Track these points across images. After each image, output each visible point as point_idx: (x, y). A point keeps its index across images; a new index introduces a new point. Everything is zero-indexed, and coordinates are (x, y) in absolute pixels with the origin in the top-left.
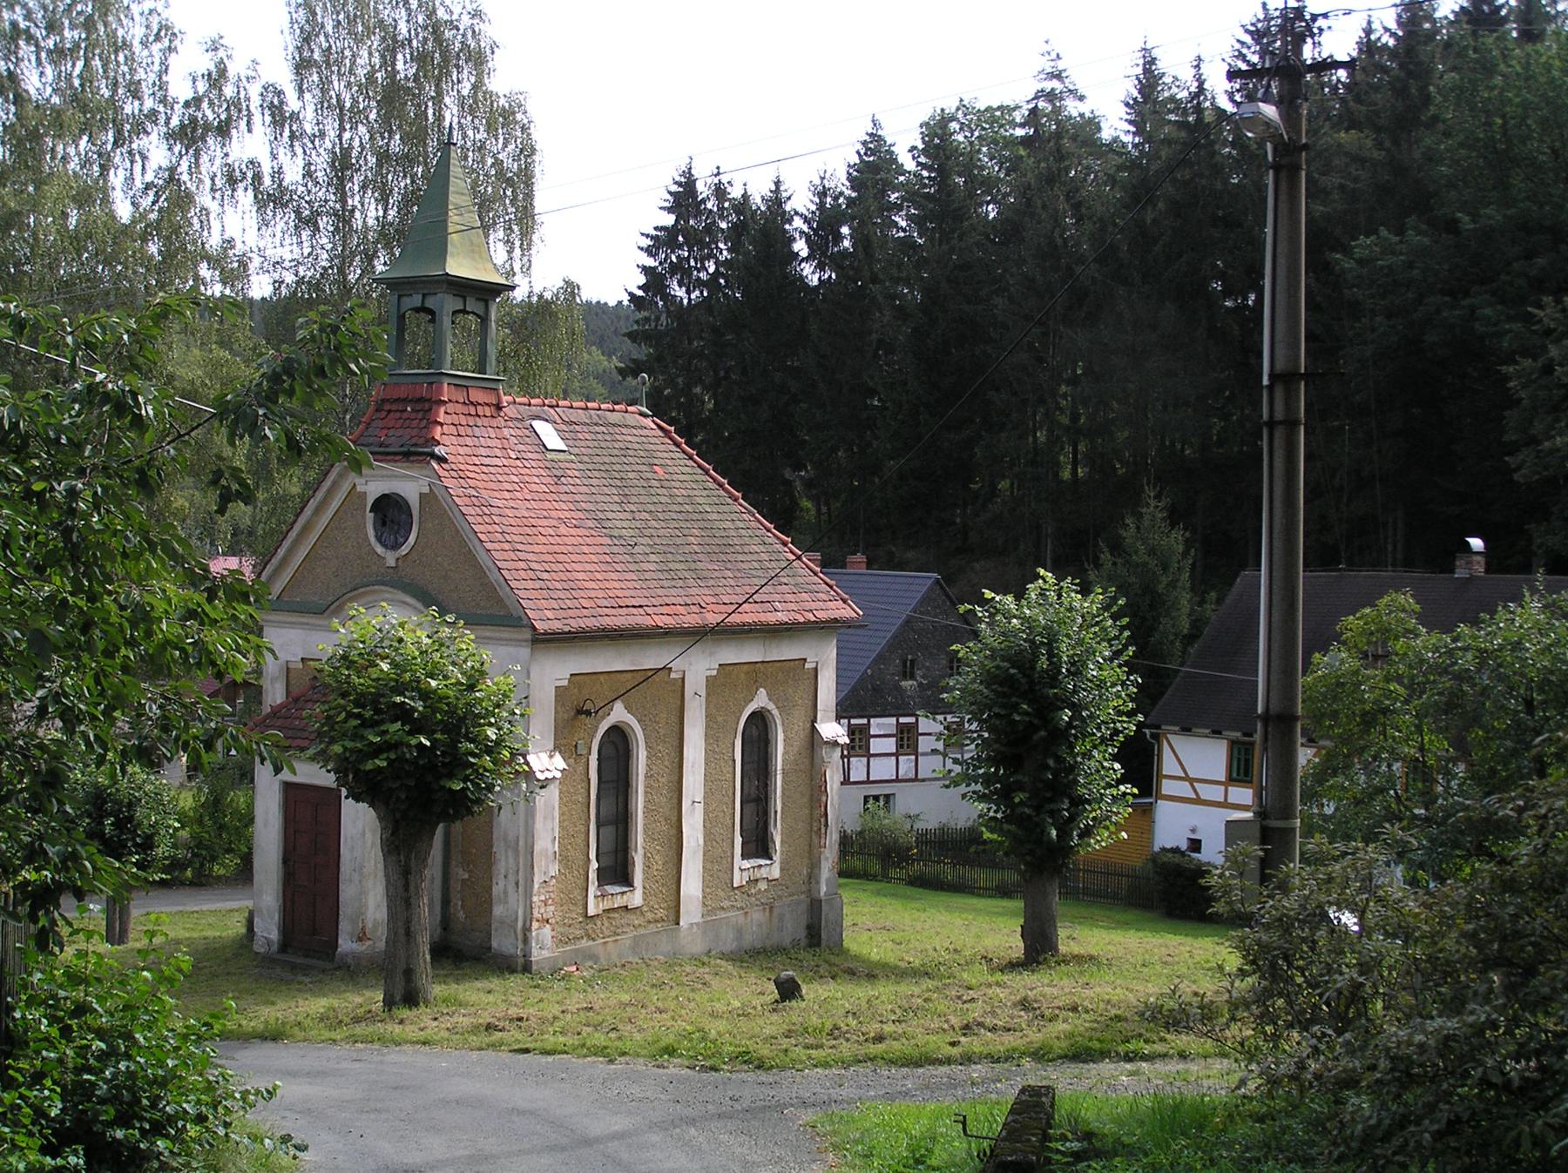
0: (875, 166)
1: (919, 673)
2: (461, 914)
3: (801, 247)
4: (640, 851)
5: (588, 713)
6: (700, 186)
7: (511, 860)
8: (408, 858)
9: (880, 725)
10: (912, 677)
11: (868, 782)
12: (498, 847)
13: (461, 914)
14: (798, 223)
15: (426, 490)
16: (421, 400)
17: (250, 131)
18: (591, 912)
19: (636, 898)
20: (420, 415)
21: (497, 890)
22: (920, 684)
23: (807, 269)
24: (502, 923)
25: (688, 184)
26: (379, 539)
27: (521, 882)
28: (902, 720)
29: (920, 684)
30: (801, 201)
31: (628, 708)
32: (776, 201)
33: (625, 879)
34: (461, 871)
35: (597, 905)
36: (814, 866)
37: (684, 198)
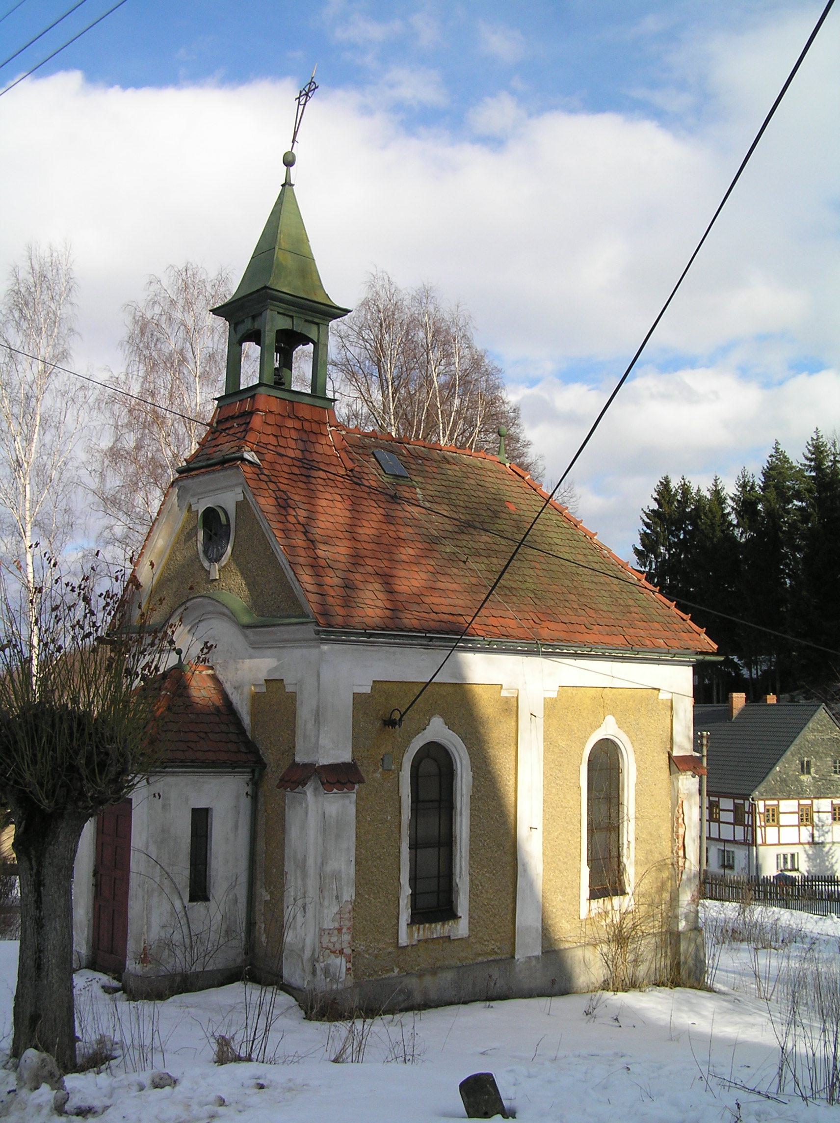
1: (812, 770)
2: (264, 938)
3: (733, 518)
4: (466, 878)
6: (672, 485)
7: (300, 882)
8: (40, 864)
9: (788, 806)
10: (809, 773)
11: (779, 844)
13: (264, 938)
14: (729, 501)
15: (240, 498)
17: (605, 766)
18: (403, 940)
19: (461, 928)
21: (289, 912)
22: (814, 778)
23: (737, 532)
25: (665, 484)
26: (206, 552)
28: (802, 802)
29: (814, 778)
30: (730, 489)
31: (450, 725)
32: (717, 493)
33: (446, 911)
34: (264, 893)
35: (410, 935)
36: (674, 900)
37: (664, 492)
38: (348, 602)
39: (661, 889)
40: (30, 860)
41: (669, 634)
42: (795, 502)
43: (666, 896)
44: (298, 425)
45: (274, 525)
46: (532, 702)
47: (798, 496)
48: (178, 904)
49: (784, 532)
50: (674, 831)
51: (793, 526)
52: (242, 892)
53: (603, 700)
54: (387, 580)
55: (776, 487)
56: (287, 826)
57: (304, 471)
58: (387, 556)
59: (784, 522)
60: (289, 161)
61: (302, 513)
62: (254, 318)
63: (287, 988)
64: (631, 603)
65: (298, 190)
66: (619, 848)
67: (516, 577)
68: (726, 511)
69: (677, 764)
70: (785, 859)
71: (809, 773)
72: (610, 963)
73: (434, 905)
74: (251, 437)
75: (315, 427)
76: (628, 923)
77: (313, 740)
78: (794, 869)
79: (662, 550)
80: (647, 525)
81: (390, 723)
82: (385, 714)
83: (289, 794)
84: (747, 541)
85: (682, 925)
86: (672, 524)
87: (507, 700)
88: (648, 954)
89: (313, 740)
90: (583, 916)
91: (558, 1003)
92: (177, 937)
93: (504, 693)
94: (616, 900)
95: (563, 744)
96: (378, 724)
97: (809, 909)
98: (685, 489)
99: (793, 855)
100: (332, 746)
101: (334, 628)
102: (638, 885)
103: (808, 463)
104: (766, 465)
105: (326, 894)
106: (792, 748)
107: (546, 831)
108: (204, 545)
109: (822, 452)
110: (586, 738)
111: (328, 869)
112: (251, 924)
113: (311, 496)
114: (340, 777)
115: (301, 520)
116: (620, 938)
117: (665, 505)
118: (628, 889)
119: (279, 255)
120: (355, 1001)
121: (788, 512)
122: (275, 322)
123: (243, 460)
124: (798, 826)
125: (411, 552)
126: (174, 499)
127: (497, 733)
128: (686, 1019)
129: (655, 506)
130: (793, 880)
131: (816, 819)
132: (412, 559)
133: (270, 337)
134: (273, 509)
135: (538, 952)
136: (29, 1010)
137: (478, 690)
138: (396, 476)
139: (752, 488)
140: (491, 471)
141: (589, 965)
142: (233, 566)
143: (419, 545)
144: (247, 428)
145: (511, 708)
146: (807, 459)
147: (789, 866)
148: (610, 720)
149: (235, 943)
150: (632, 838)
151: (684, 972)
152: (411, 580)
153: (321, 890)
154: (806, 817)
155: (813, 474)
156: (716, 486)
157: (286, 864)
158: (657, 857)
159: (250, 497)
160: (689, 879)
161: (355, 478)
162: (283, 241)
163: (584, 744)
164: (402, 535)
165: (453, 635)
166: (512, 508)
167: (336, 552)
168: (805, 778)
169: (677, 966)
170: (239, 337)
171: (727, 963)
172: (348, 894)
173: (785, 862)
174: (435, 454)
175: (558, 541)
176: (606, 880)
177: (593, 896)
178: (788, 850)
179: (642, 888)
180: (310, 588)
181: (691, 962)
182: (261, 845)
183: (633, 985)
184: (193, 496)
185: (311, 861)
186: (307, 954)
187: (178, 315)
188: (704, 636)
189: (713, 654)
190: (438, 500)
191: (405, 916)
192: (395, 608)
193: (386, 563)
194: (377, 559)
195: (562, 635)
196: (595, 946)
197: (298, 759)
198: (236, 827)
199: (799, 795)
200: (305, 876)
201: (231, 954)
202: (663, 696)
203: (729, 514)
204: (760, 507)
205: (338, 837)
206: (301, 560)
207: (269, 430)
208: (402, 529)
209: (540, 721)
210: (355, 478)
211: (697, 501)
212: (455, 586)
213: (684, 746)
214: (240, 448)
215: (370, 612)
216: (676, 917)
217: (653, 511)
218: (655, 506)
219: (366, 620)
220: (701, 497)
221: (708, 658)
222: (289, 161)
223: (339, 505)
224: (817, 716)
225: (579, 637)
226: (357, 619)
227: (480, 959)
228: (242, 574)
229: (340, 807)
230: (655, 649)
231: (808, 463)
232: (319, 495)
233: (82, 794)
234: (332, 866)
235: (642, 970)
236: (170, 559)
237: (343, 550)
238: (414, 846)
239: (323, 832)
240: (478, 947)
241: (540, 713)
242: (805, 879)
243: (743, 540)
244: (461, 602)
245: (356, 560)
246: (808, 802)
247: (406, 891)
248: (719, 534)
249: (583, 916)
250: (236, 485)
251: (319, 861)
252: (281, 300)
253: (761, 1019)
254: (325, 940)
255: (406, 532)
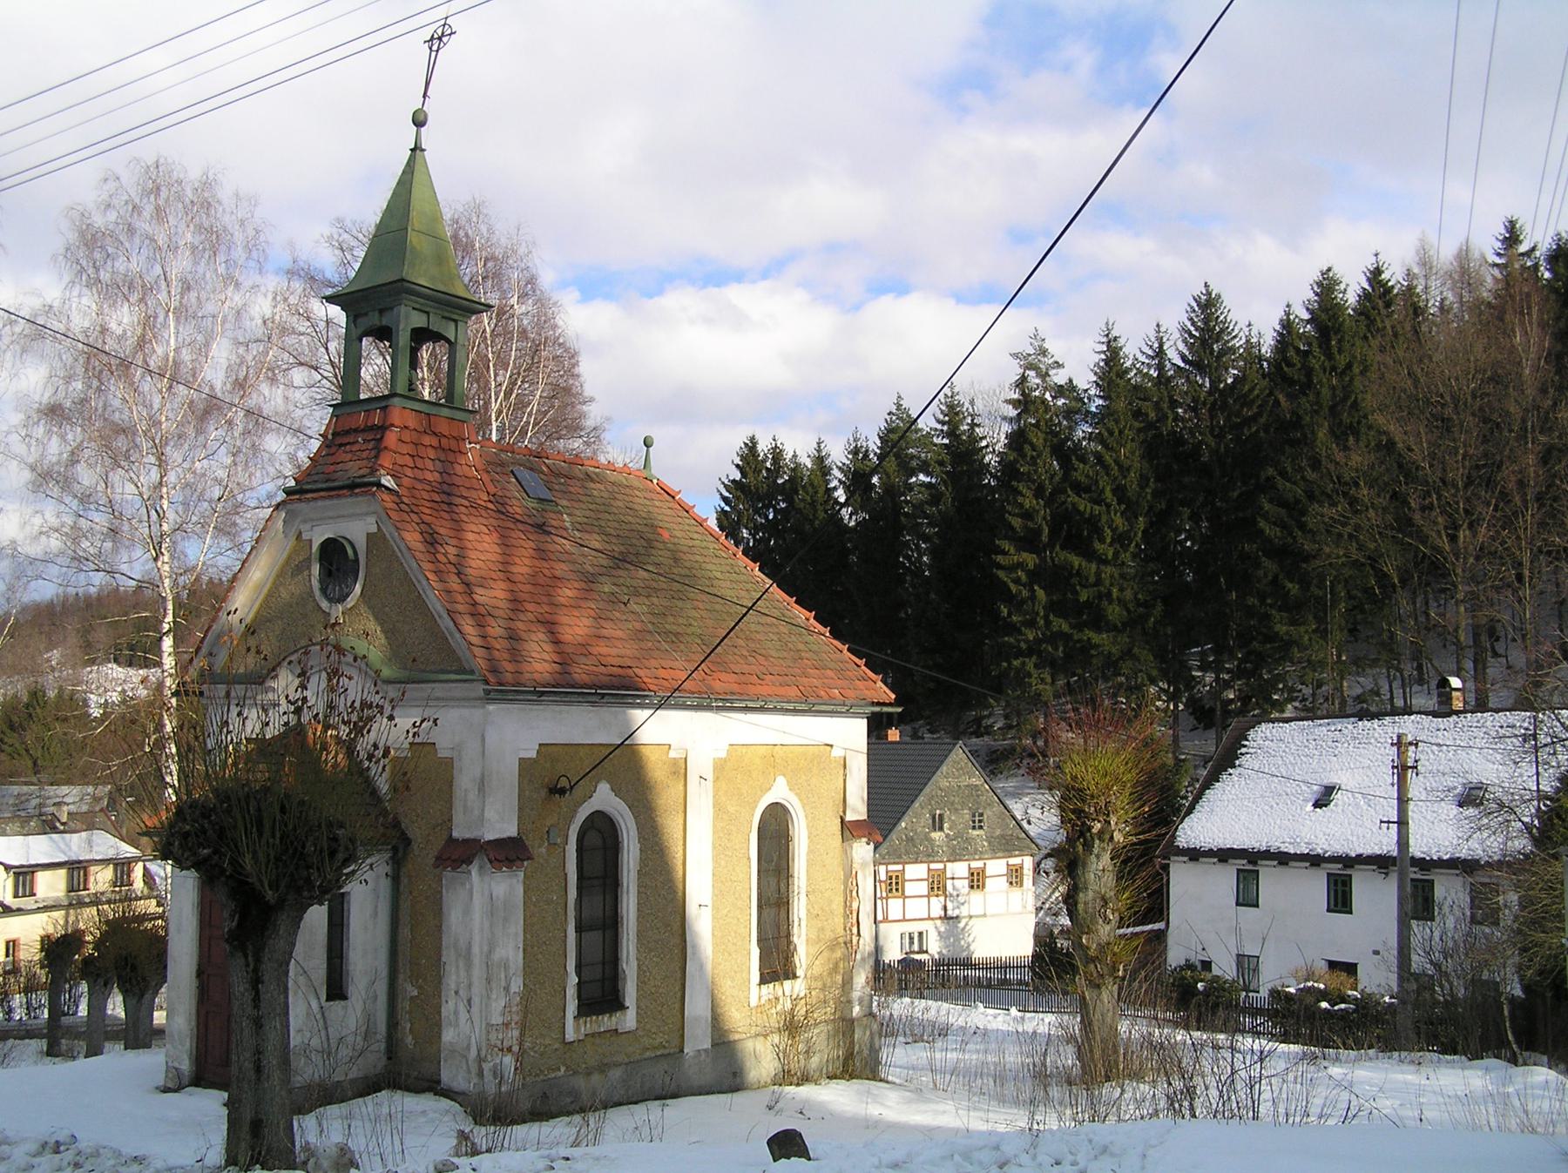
0: (898, 435)
3: (841, 495)
4: (634, 964)
5: (562, 792)
6: (759, 448)
7: (462, 973)
8: (258, 960)
9: (917, 871)
10: (941, 829)
11: (904, 920)
12: (448, 956)
13: (409, 1040)
14: (836, 472)
15: (374, 529)
16: (372, 428)
17: (775, 832)
18: (570, 1035)
19: (629, 1020)
20: (371, 445)
21: (447, 1009)
22: (947, 836)
23: (845, 513)
24: (454, 1051)
25: (752, 446)
26: (324, 591)
27: (476, 1000)
28: (933, 866)
29: (947, 836)
30: (838, 454)
31: (617, 791)
32: (820, 460)
33: (613, 1002)
34: (409, 987)
35: (577, 1030)
36: (847, 983)
37: (750, 451)
38: (516, 655)
39: (835, 969)
40: (246, 956)
41: (844, 683)
42: (922, 477)
43: (839, 978)
44: (435, 442)
45: (426, 566)
46: (701, 765)
47: (925, 468)
48: (314, 1004)
49: (906, 514)
50: (847, 905)
51: (918, 507)
52: (382, 988)
53: (774, 760)
54: (550, 626)
55: (897, 456)
56: (445, 910)
57: (445, 498)
58: (545, 599)
59: (907, 502)
60: (419, 121)
61: (452, 550)
62: (381, 312)
63: (448, 1094)
64: (801, 646)
65: (430, 156)
66: (789, 924)
67: (681, 621)
68: (832, 485)
69: (849, 830)
70: (911, 938)
71: (941, 829)
72: (782, 1055)
73: (602, 995)
74: (386, 460)
75: (453, 443)
76: (801, 1011)
77: (476, 812)
78: (921, 951)
79: (745, 533)
80: (725, 499)
81: (557, 791)
82: (551, 779)
83: (448, 874)
84: (858, 524)
85: (856, 1010)
86: (759, 500)
87: (675, 761)
88: (821, 1046)
89: (476, 812)
90: (754, 1003)
91: (737, 1096)
92: (315, 1042)
93: (672, 754)
94: (787, 984)
95: (732, 809)
96: (544, 793)
97: (954, 1000)
98: (777, 453)
99: (921, 934)
100: (500, 822)
101: (503, 687)
102: (810, 967)
103: (939, 427)
104: (883, 425)
105: (494, 985)
106: (921, 798)
107: (716, 909)
108: (321, 581)
109: (957, 414)
110: (756, 802)
111: (496, 956)
112: (393, 1024)
113: (458, 529)
114: (508, 853)
115: (452, 558)
116: (792, 1027)
117: (750, 475)
118: (799, 972)
119: (412, 237)
120: (525, 1106)
121: (910, 488)
122: (410, 319)
123: (379, 485)
124: (928, 896)
125: (568, 593)
126: (280, 524)
127: (666, 798)
128: (874, 1111)
129: (737, 476)
130: (921, 964)
131: (949, 888)
132: (572, 602)
133: (404, 338)
134: (420, 547)
135: (707, 1045)
136: (248, 1115)
137: (645, 751)
138: (541, 500)
139: (866, 455)
140: (638, 489)
141: (762, 1058)
142: (363, 609)
143: (576, 585)
144: (379, 448)
145: (680, 770)
146: (938, 421)
147: (916, 947)
148: (781, 781)
149: (374, 1047)
150: (803, 914)
151: (858, 1064)
152: (576, 627)
153: (489, 981)
154: (937, 885)
155: (946, 441)
156: (819, 451)
157: (444, 953)
158: (829, 935)
159: (388, 530)
160: (863, 959)
161: (500, 506)
162: (416, 220)
163: (754, 809)
164: (558, 573)
165: (622, 690)
166: (666, 534)
167: (493, 595)
168: (936, 835)
169: (849, 1056)
170: (360, 331)
171: (897, 1056)
172: (517, 985)
173: (911, 943)
174: (577, 470)
175: (718, 575)
176: (777, 966)
177: (764, 980)
178: (915, 928)
179: (817, 970)
180: (474, 640)
181: (866, 1052)
182: (405, 932)
183: (805, 1079)
184: (305, 521)
185: (476, 950)
186: (473, 1053)
187: (144, 225)
188: (880, 684)
189: (890, 704)
190: (588, 528)
191: (572, 1007)
192: (564, 661)
193: (547, 608)
194: (535, 600)
195: (735, 688)
196: (765, 1036)
197: (455, 834)
198: (375, 914)
199: (929, 856)
200: (469, 965)
201: (375, 1059)
202: (837, 753)
203: (835, 488)
204: (875, 480)
205: (506, 919)
206: (460, 608)
207: (405, 449)
208: (555, 565)
209: (710, 784)
210: (500, 506)
211: (793, 470)
212: (619, 633)
213: (858, 809)
214: (373, 471)
215: (538, 666)
216: (850, 1002)
217: (734, 481)
218: (737, 476)
219: (536, 676)
220: (798, 465)
221: (886, 709)
222: (419, 121)
223: (487, 538)
224: (953, 756)
225: (752, 690)
226: (527, 676)
227: (648, 1054)
228: (376, 618)
229: (507, 886)
230: (831, 700)
231: (939, 427)
232: (465, 526)
233: (308, 880)
234: (499, 954)
235: (815, 1061)
236: (270, 595)
237: (501, 594)
238: (579, 929)
239: (488, 921)
240: (646, 1041)
241: (710, 776)
242: (938, 963)
243: (852, 524)
244: (628, 652)
245: (516, 604)
246: (941, 866)
247: (573, 979)
248: (821, 515)
249: (754, 1003)
250: (367, 514)
251: (486, 948)
252: (419, 295)
253: (949, 1106)
254: (493, 1036)
255: (561, 569)
